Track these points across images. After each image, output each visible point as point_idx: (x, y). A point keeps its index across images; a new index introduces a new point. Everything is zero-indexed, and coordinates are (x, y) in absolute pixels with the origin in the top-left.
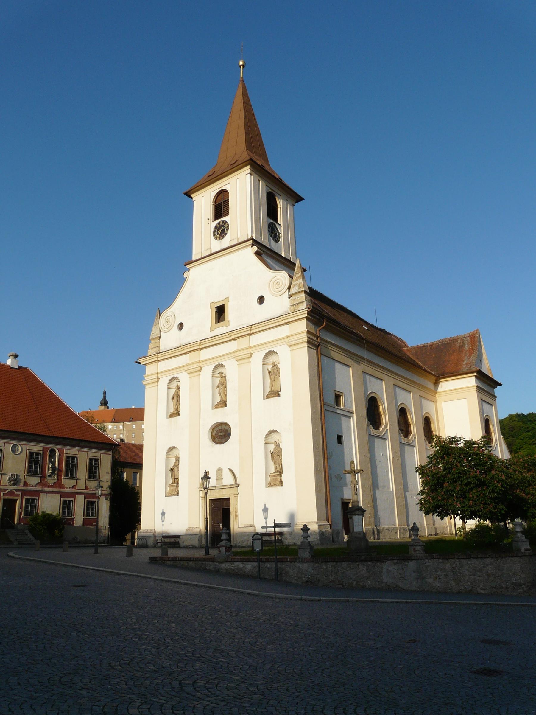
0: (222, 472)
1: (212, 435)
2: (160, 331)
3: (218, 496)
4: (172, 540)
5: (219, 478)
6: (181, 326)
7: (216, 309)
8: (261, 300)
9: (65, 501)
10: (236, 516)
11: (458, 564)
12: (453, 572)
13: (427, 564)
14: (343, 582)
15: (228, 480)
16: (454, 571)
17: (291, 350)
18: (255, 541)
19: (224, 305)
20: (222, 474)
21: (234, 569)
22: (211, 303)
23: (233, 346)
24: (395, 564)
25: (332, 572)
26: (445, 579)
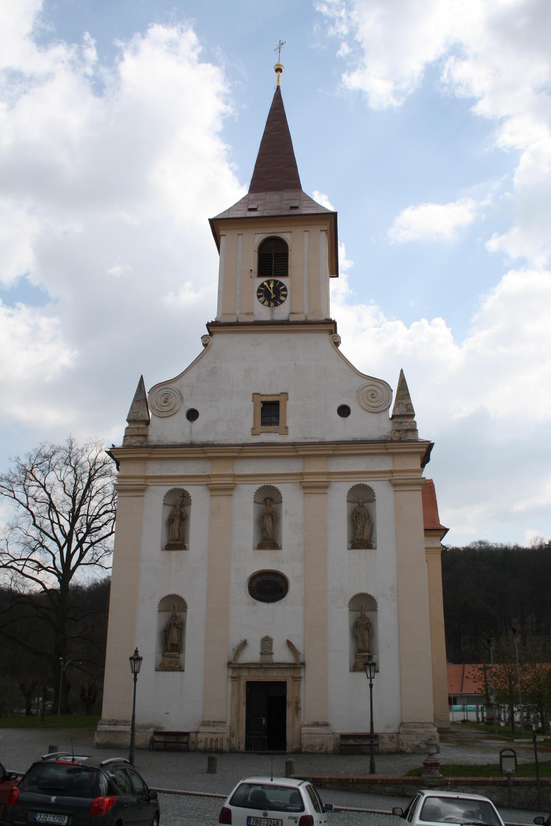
0: (271, 644)
3: (263, 678)
4: (173, 739)
7: (262, 404)
8: (344, 411)
10: (298, 709)
18: (503, 759)
19: (434, 443)
20: (271, 647)
23: (295, 466)
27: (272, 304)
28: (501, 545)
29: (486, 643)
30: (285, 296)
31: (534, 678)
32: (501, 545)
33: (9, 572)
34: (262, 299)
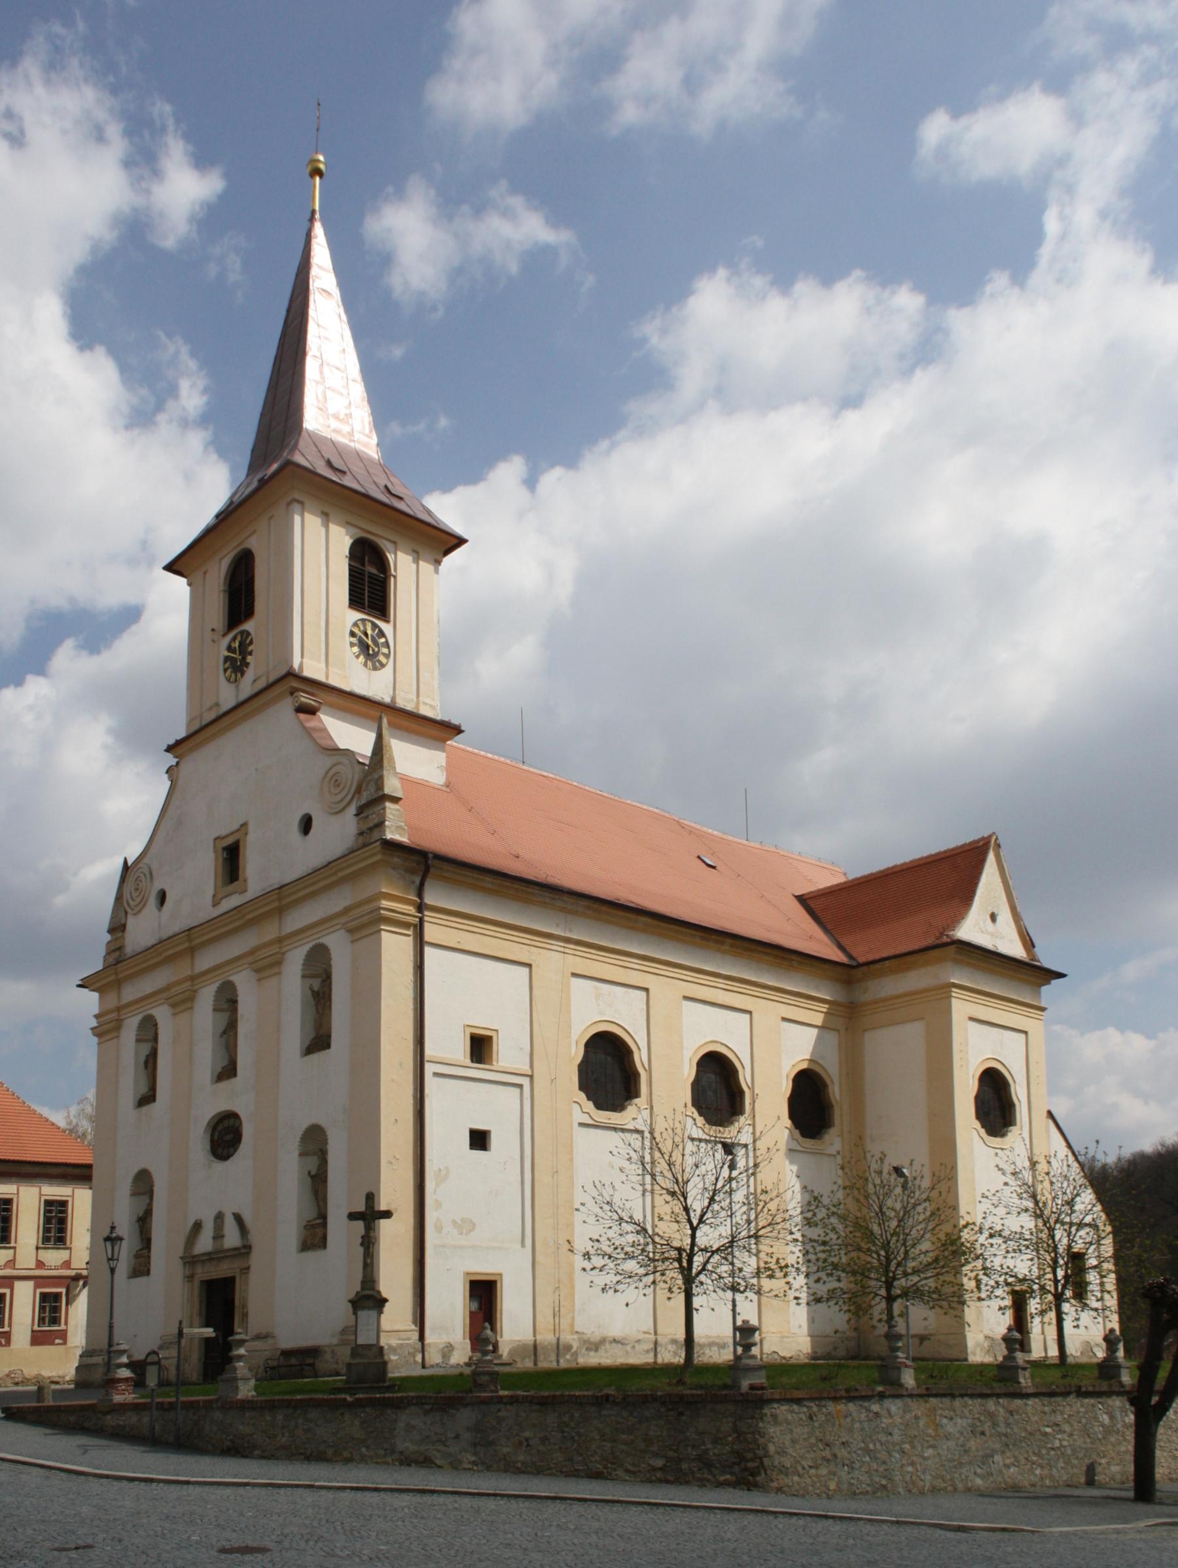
1: (212, 1142)
2: (126, 913)
5: (218, 1236)
6: (162, 897)
8: (306, 825)
9: (44, 1297)
11: (577, 1415)
12: (563, 1432)
13: (503, 1414)
14: (305, 1449)
15: (232, 1238)
16: (566, 1429)
17: (352, 942)
21: (124, 1426)
22: (216, 839)
24: (426, 1413)
25: (283, 1428)
26: (541, 1448)
30: (387, 656)
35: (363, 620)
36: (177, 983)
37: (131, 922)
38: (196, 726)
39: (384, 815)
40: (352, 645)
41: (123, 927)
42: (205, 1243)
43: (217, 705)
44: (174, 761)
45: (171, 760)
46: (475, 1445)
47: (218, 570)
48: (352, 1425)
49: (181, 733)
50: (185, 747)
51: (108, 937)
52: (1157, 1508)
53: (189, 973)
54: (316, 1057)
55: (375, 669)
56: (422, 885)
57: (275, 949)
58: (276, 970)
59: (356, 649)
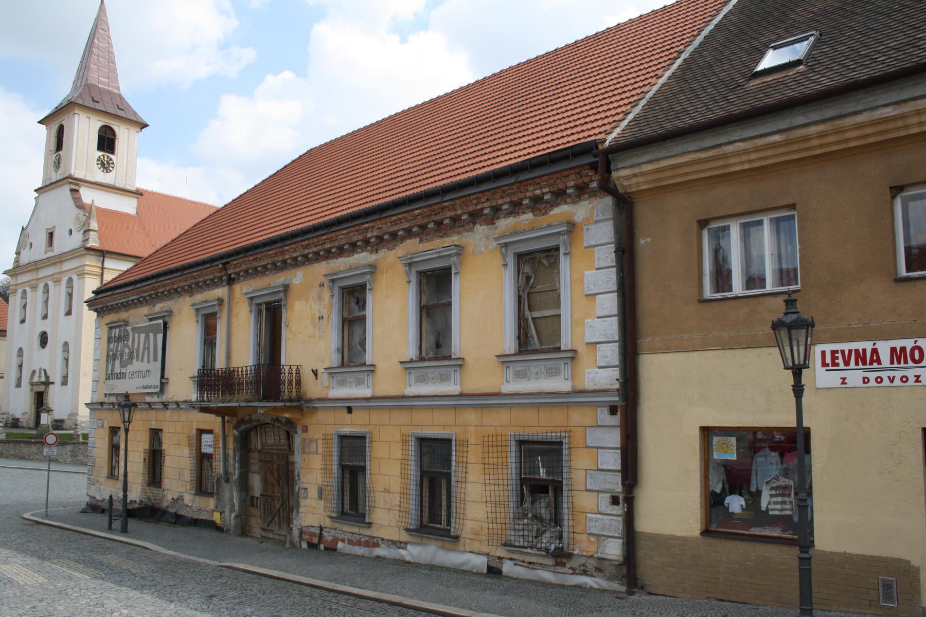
6: (31, 244)
27: (105, 171)
28: (915, 285)
29: (107, 38)
30: (113, 167)
31: (281, 540)
32: (915, 285)
33: (283, 442)
34: (99, 166)
35: (103, 156)
36: (32, 280)
37: (22, 252)
38: (48, 183)
39: (89, 237)
40: (98, 164)
41: (20, 253)
42: (36, 379)
43: (50, 179)
44: (37, 195)
45: (36, 195)
46: (71, 456)
47: (55, 128)
48: (34, 449)
49: (40, 186)
50: (42, 190)
51: (15, 256)
52: (708, 509)
53: (36, 277)
54: (68, 317)
55: (107, 172)
56: (103, 261)
57: (58, 276)
58: (59, 283)
59: (99, 166)
